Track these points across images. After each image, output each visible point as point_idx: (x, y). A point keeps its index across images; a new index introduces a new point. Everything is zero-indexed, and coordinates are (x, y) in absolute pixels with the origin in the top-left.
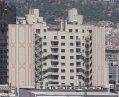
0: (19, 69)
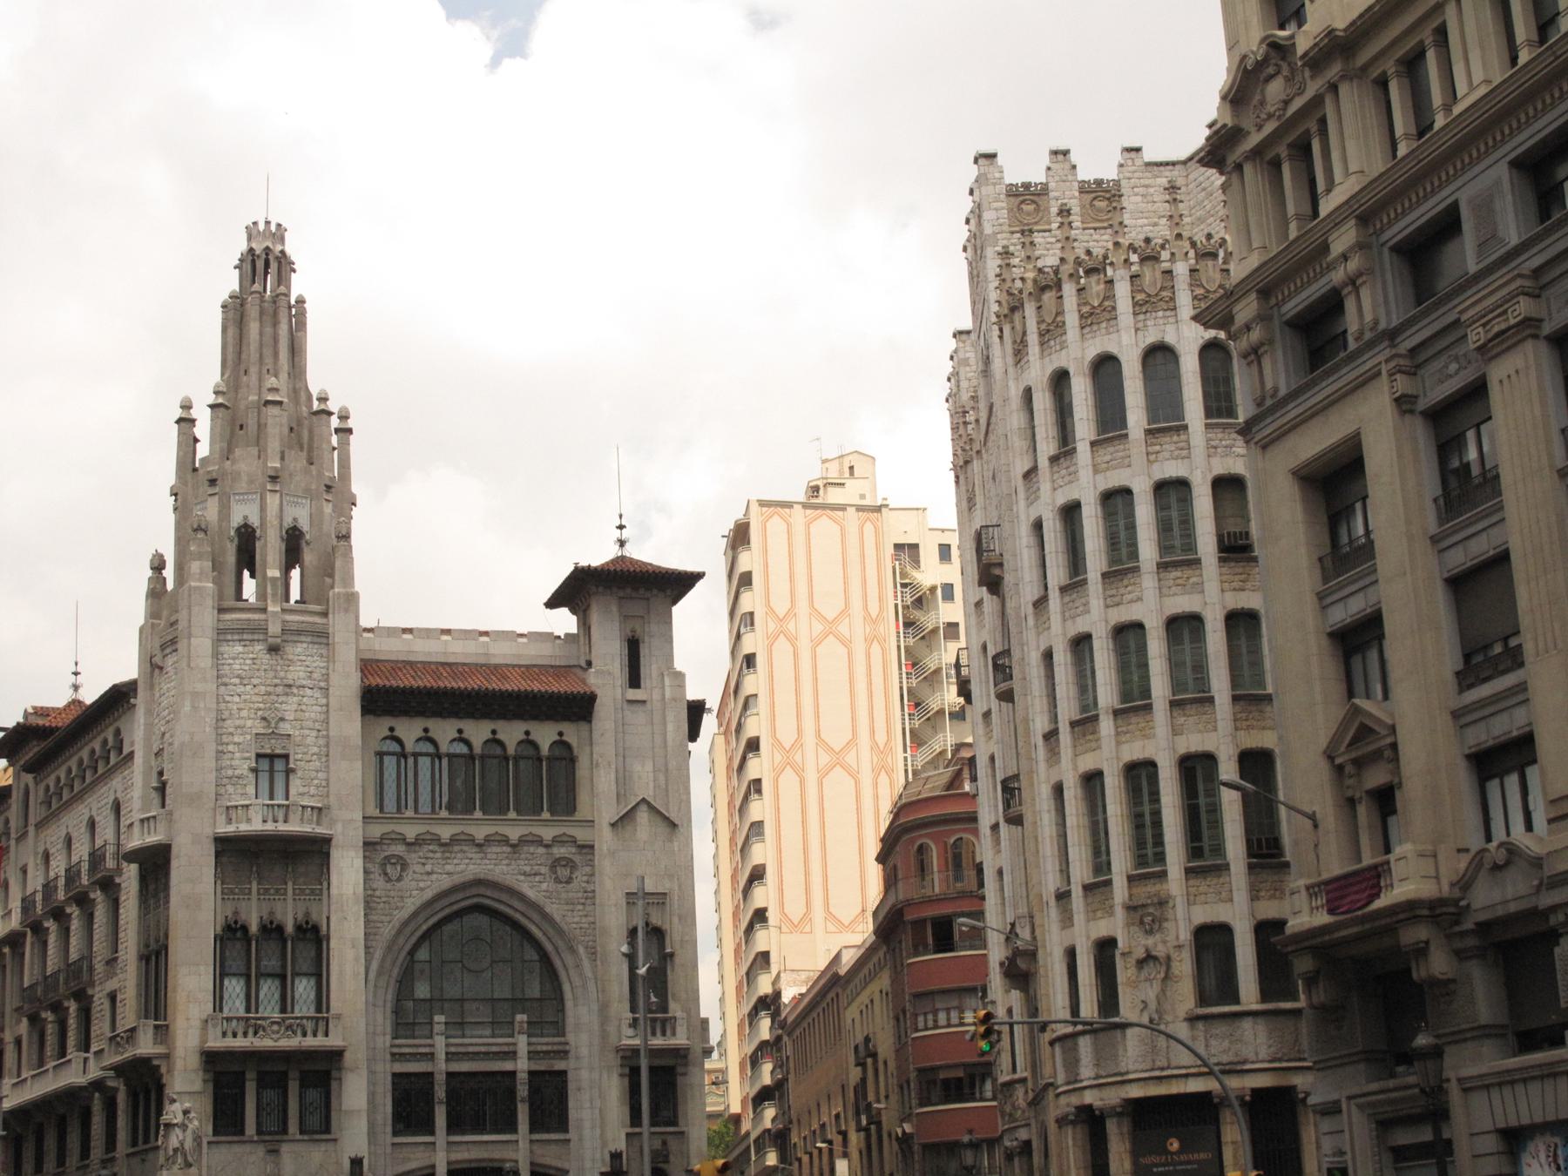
0: (816, 643)
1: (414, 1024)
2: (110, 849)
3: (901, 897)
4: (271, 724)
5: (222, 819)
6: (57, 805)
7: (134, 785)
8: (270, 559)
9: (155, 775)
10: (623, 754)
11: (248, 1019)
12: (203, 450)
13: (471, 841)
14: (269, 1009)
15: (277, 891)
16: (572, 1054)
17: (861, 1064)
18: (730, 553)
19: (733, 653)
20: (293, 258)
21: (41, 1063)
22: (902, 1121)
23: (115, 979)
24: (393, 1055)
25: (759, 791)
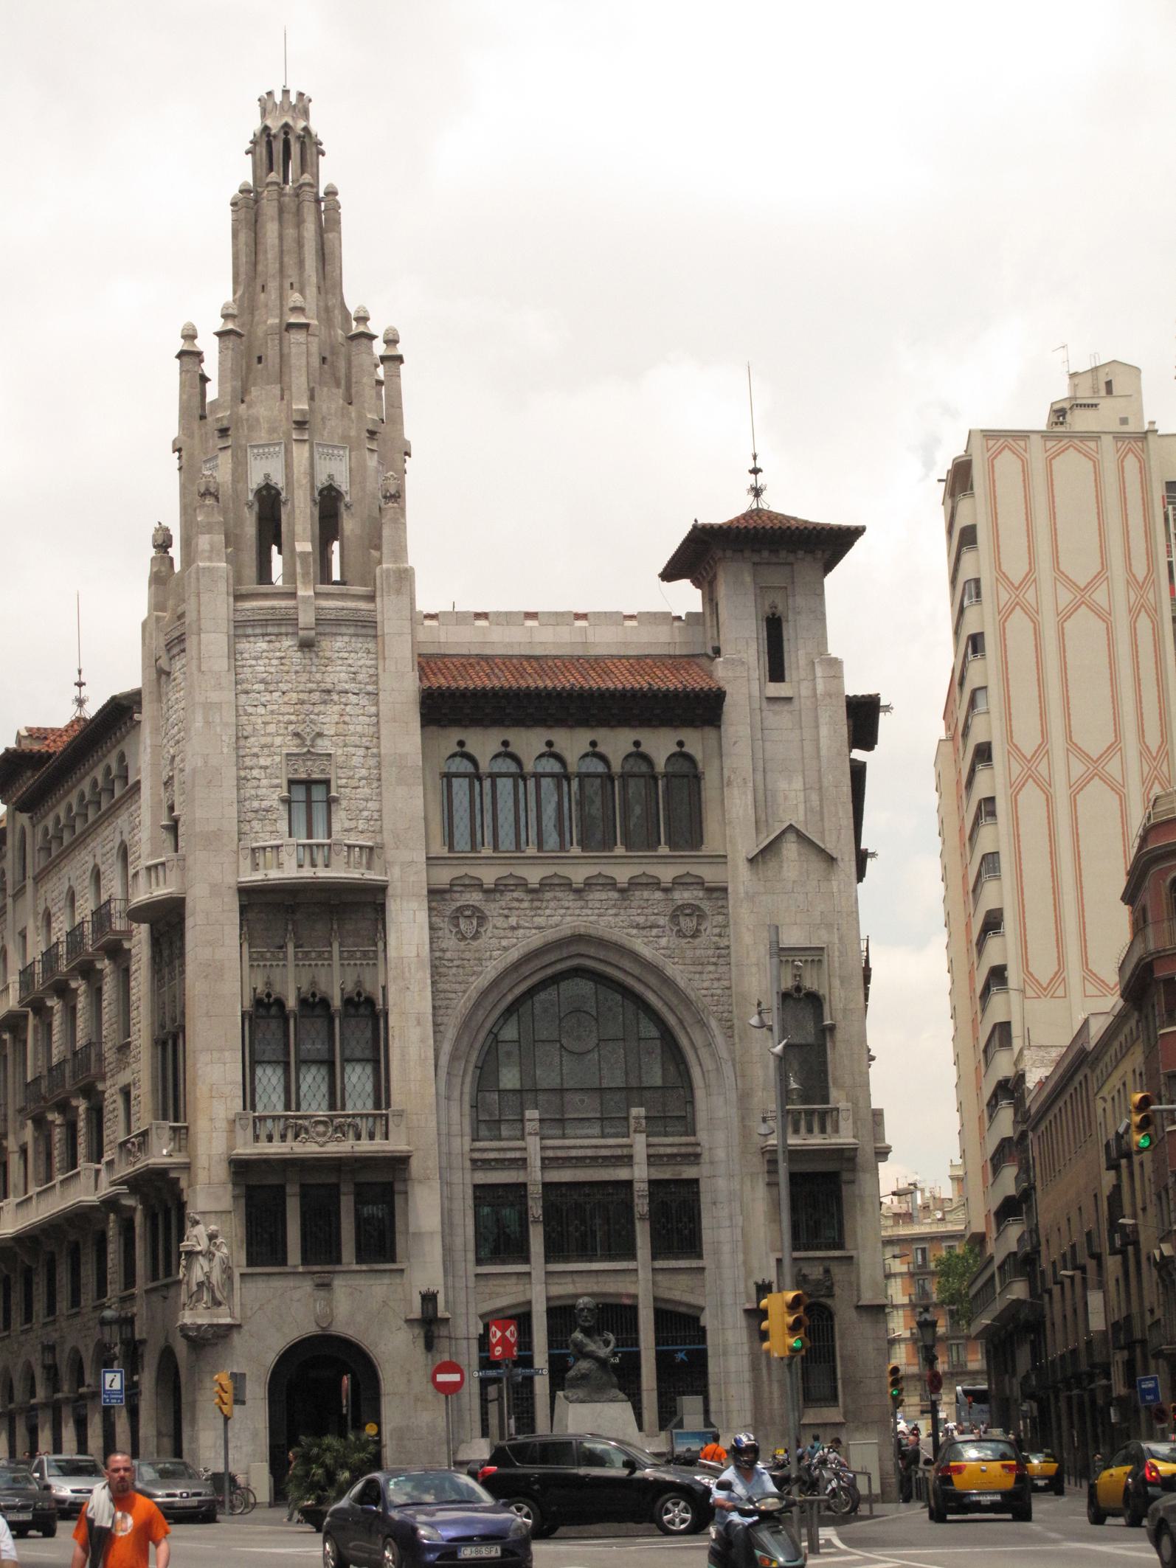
0: (1063, 617)
1: (499, 1121)
2: (117, 907)
3: (1152, 947)
4: (307, 743)
5: (246, 864)
6: (58, 850)
7: (143, 821)
8: (299, 529)
9: (165, 811)
10: (763, 767)
11: (287, 1118)
12: (212, 392)
13: (567, 885)
14: (314, 1106)
15: (320, 954)
16: (705, 1157)
17: (1113, 1166)
18: (949, 502)
19: (957, 633)
20: (320, 138)
21: (49, 1178)
22: (1162, 1240)
23: (128, 1071)
24: (473, 1161)
25: (992, 814)
